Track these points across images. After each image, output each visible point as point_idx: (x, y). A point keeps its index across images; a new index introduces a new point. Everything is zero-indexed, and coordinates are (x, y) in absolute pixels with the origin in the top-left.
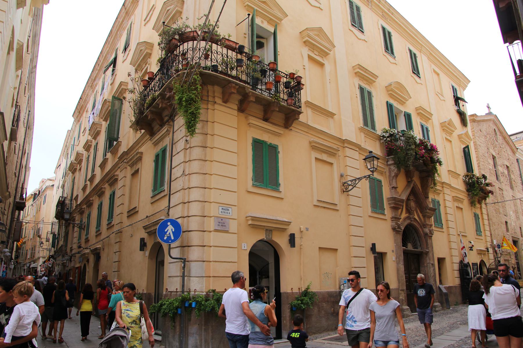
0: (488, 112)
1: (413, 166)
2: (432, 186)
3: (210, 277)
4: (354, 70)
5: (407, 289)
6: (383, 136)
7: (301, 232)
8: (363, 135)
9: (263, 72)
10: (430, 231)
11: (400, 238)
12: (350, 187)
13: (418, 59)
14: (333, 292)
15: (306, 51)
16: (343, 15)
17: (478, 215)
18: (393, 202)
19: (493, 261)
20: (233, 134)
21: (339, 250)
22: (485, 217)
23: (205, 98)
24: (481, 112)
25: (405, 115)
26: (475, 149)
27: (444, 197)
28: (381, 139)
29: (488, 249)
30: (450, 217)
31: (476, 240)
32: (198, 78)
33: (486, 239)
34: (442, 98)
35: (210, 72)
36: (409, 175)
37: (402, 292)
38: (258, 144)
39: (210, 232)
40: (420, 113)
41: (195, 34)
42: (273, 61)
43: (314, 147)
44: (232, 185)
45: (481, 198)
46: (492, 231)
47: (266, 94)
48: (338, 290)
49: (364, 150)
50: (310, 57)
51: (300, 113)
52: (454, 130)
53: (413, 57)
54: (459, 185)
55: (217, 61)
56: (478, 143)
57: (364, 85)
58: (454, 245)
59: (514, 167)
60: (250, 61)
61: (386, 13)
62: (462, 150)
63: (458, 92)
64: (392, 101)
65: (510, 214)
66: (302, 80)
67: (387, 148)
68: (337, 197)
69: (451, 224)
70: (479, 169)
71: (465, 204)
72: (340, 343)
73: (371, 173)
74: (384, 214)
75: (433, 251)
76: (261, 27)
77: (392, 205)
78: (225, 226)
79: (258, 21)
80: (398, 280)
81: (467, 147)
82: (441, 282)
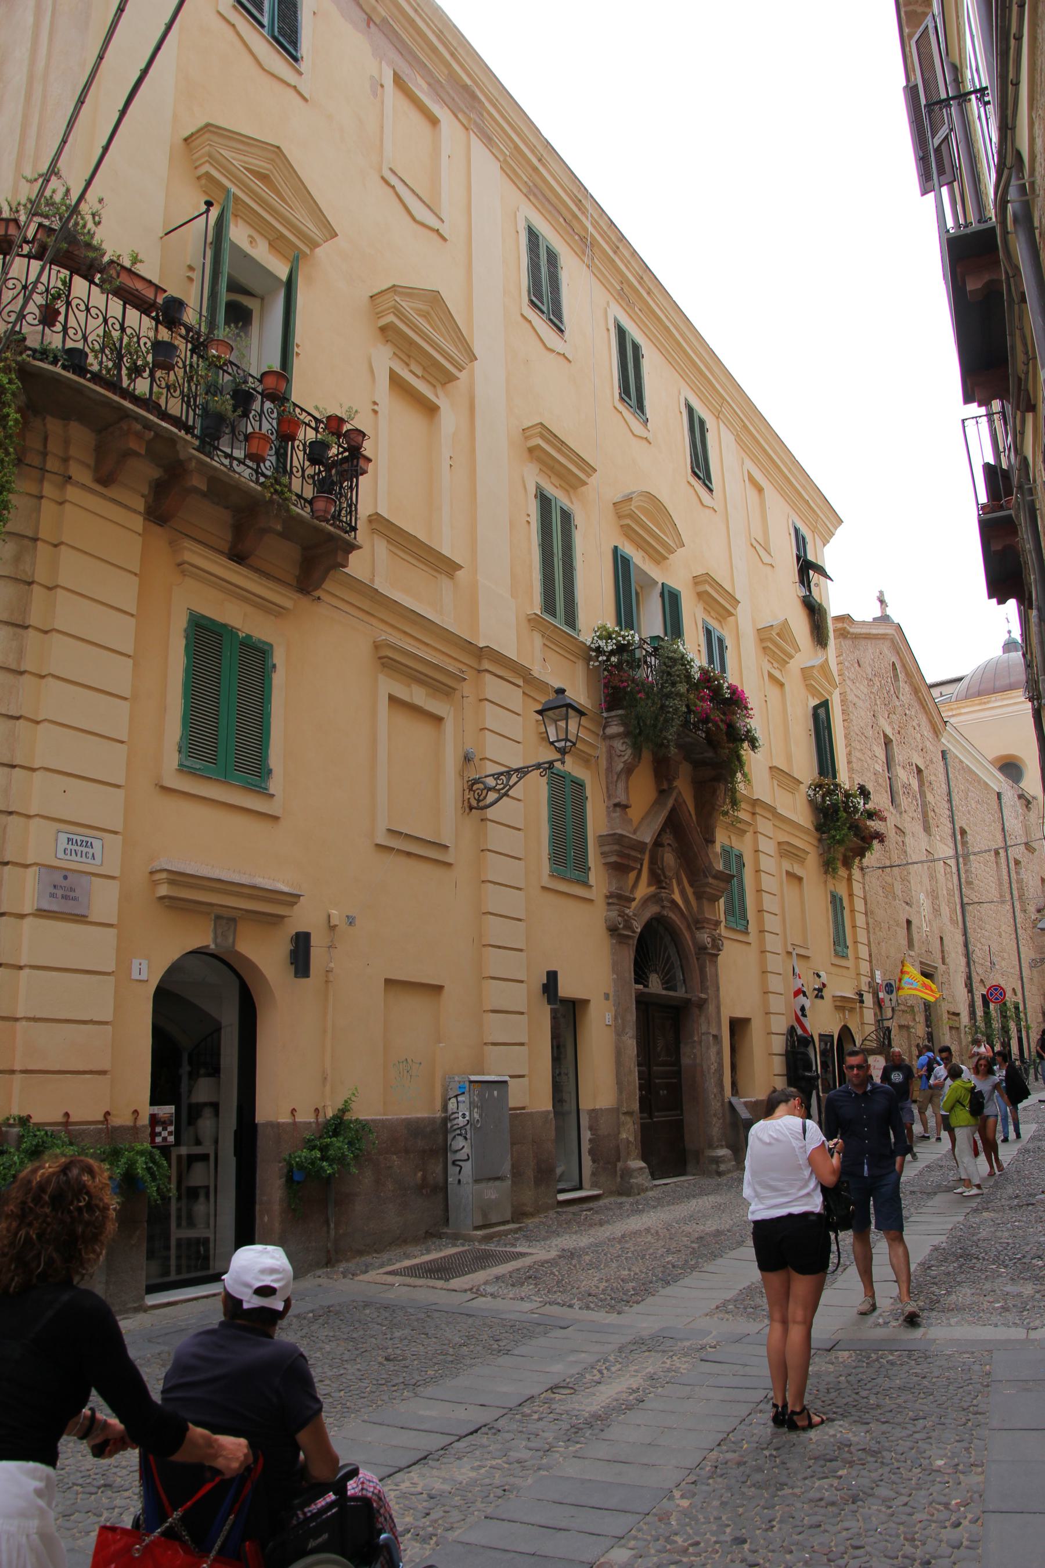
0: (879, 614)
1: (679, 746)
2: (725, 808)
3: (13, 1072)
4: (527, 438)
5: (642, 1111)
6: (599, 650)
7: (332, 928)
8: (538, 640)
9: (243, 399)
10: (713, 940)
11: (628, 956)
12: (492, 796)
13: (710, 437)
14: (423, 1119)
15: (384, 359)
16: (504, 271)
17: (841, 900)
18: (616, 847)
19: (873, 1028)
20: (124, 591)
21: (446, 991)
22: (859, 905)
23: (34, 459)
24: (865, 612)
25: (662, 595)
26: (844, 712)
27: (756, 842)
28: (589, 659)
29: (861, 995)
30: (769, 903)
31: (834, 970)
32: (10, 382)
33: (857, 967)
34: (766, 559)
35: (58, 369)
36: (662, 771)
37: (628, 1119)
38: (206, 637)
39: (22, 916)
40: (707, 592)
41: (12, 230)
42: (276, 366)
43: (388, 661)
44: (110, 763)
45: (852, 850)
46: (872, 945)
47: (245, 473)
48: (439, 1114)
49: (541, 685)
50: (395, 380)
51: (352, 547)
52: (793, 652)
53: (697, 429)
54: (797, 810)
55: (85, 338)
56: (851, 697)
57: (551, 490)
58: (775, 983)
59: (936, 774)
60: (200, 356)
61: (631, 286)
62: (810, 712)
63: (809, 547)
64: (627, 549)
65: (918, 901)
66: (365, 444)
67: (606, 686)
68: (448, 823)
69: (771, 923)
70: (851, 770)
71: (810, 868)
72: (440, 1283)
73: (558, 756)
74: (586, 884)
75: (718, 996)
76: (246, 256)
77: (613, 859)
78: (75, 899)
79: (238, 233)
80: (619, 1083)
81: (825, 704)
82: (735, 1091)
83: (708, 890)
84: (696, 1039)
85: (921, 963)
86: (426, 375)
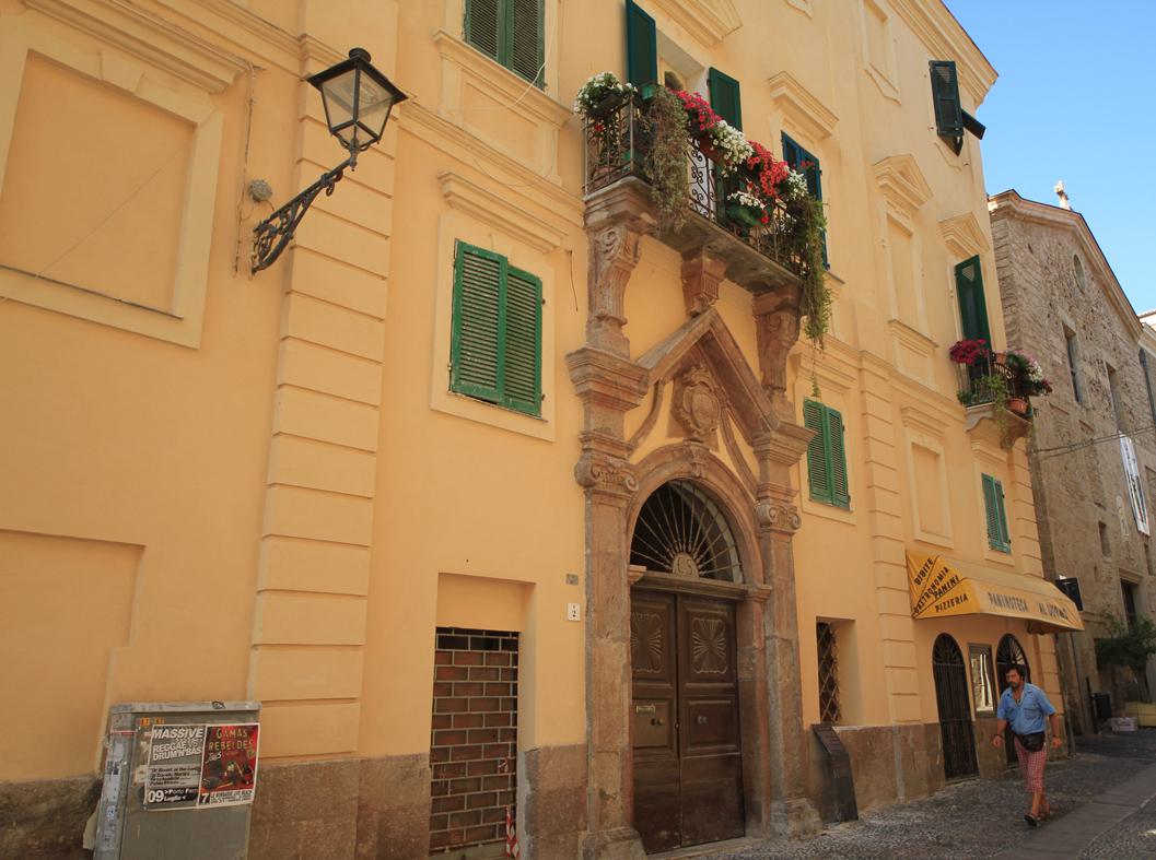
4: (773, 88)
11: (618, 536)
17: (999, 486)
27: (864, 403)
65: (1114, 504)
81: (974, 262)
83: (771, 447)
84: (756, 644)
85: (1121, 570)
86: (808, 134)
